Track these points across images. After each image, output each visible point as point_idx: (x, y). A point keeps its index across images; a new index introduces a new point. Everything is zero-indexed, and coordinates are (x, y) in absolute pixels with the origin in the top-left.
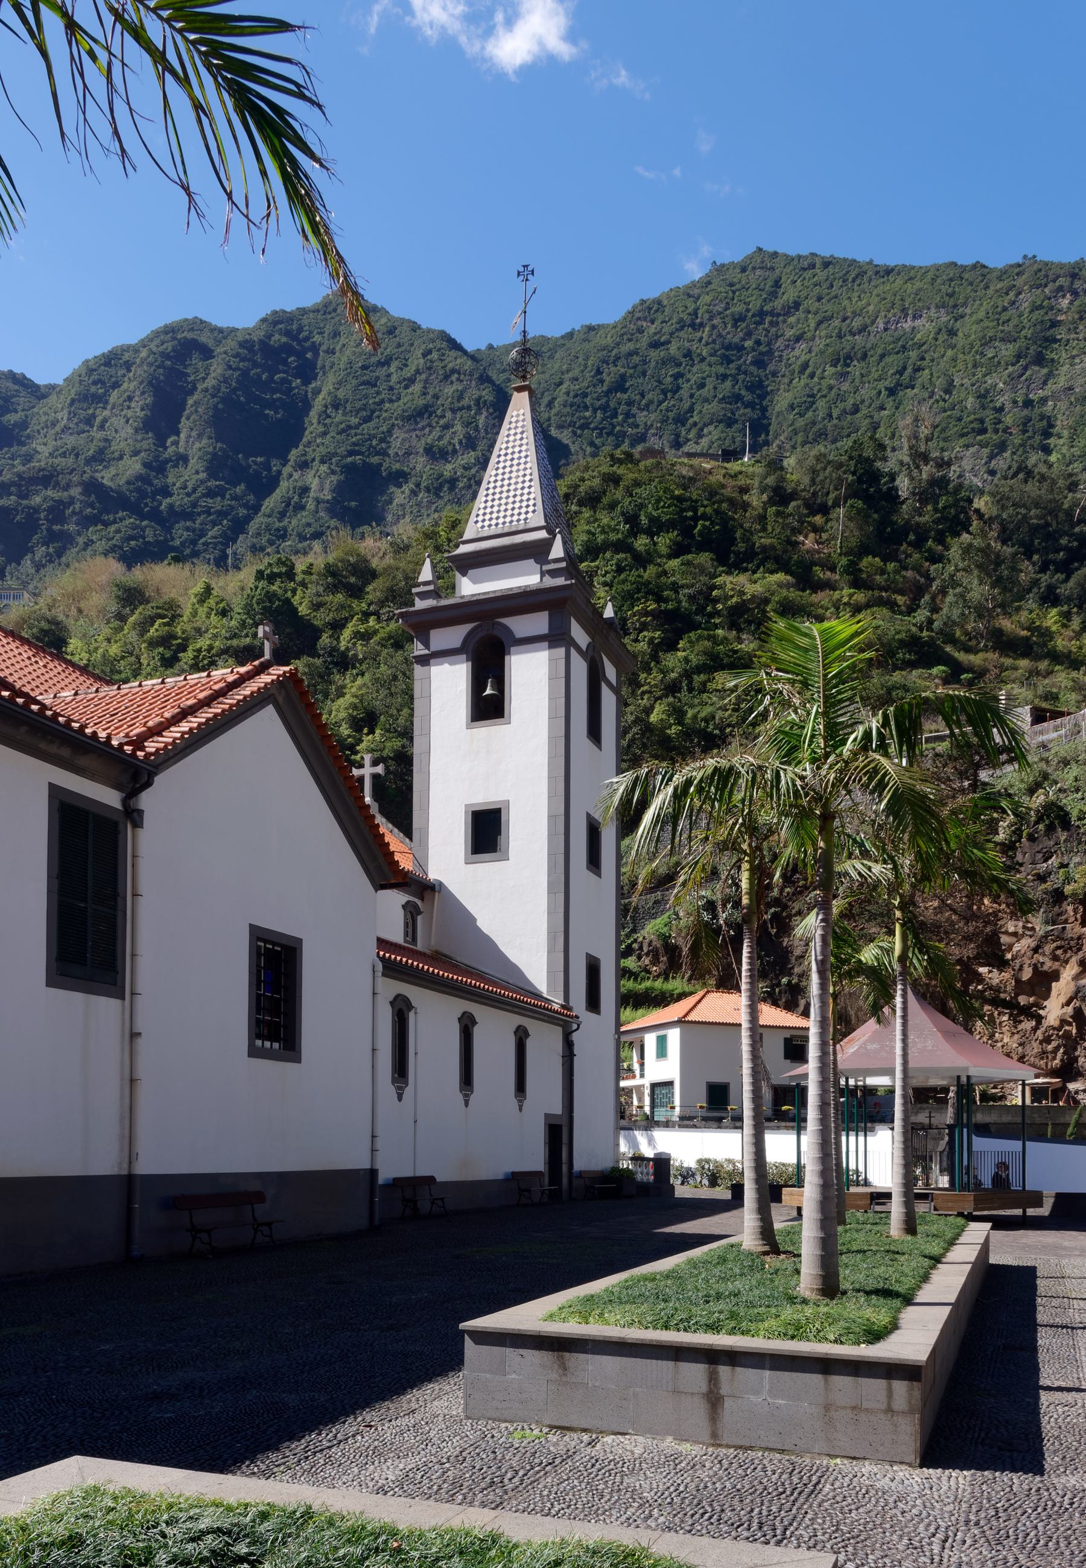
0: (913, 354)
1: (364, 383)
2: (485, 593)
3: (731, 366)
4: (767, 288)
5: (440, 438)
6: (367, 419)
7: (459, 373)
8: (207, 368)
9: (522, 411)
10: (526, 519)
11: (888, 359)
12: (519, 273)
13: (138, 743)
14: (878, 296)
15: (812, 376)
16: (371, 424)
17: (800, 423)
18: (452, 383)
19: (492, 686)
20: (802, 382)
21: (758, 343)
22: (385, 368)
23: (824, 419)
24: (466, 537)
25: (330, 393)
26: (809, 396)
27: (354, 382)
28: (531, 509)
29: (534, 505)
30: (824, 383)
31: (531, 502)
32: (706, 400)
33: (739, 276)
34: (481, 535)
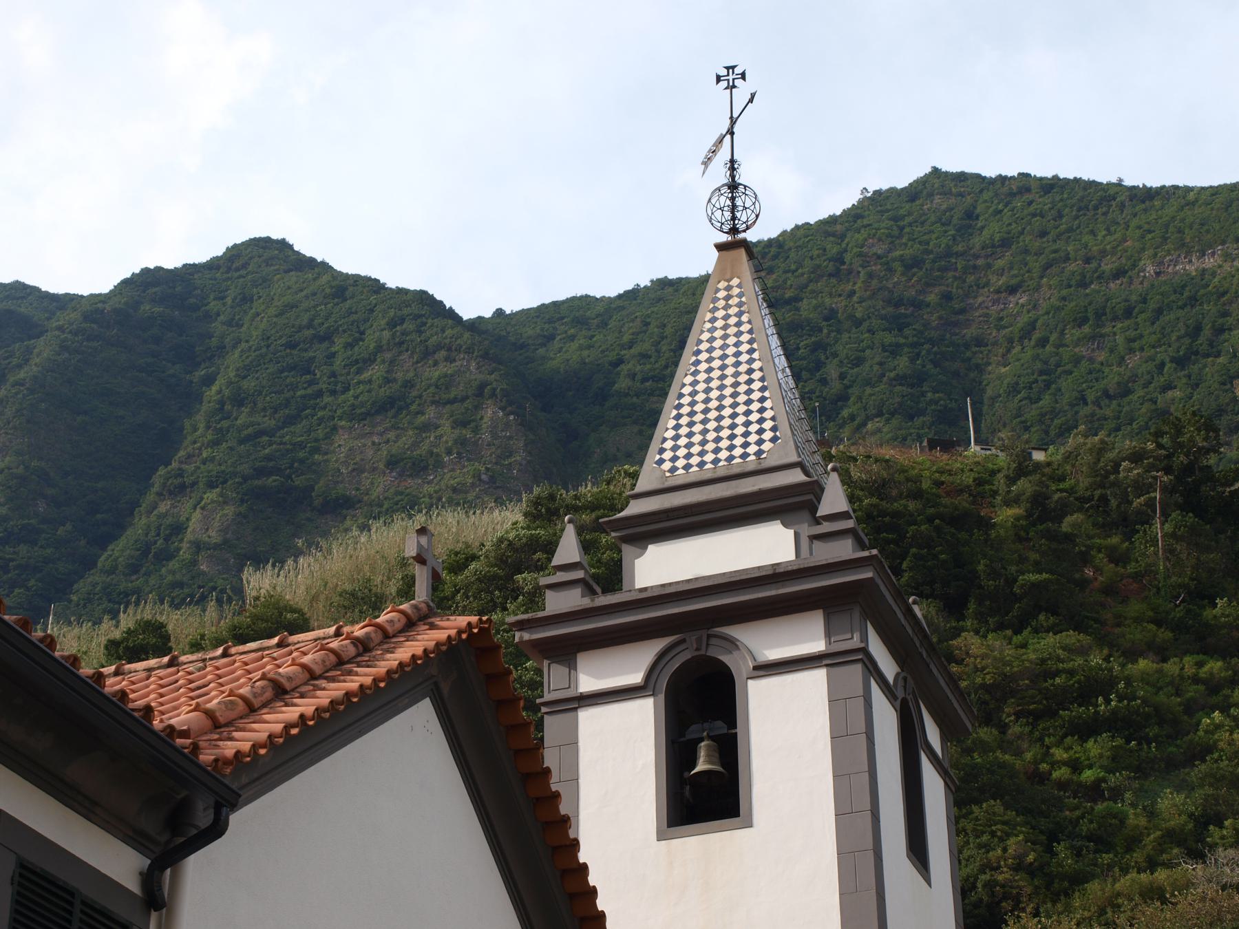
0: (1210, 308)
1: (292, 368)
2: (688, 581)
3: (907, 332)
4: (955, 221)
5: (415, 445)
6: (290, 421)
7: (449, 349)
8: (29, 351)
9: (735, 281)
10: (759, 453)
11: (1168, 317)
12: (733, 67)
13: (217, 724)
14: (1139, 227)
15: (1043, 342)
16: (298, 428)
17: (1032, 412)
18: (436, 364)
19: (708, 755)
20: (1029, 353)
21: (947, 297)
22: (326, 344)
23: (1072, 405)
24: (643, 485)
25: (230, 383)
26: (1041, 373)
27: (272, 368)
28: (768, 435)
29: (774, 429)
30: (1066, 353)
31: (768, 425)
32: (868, 383)
33: (908, 206)
34: (671, 483)
